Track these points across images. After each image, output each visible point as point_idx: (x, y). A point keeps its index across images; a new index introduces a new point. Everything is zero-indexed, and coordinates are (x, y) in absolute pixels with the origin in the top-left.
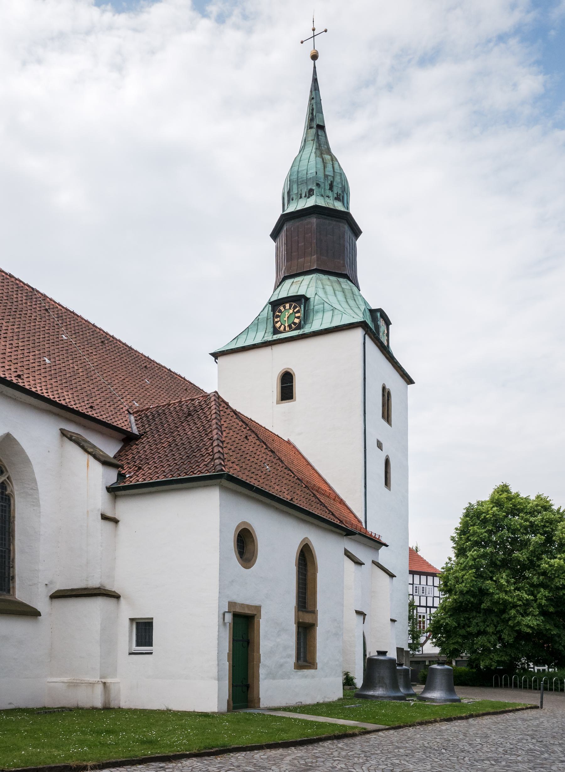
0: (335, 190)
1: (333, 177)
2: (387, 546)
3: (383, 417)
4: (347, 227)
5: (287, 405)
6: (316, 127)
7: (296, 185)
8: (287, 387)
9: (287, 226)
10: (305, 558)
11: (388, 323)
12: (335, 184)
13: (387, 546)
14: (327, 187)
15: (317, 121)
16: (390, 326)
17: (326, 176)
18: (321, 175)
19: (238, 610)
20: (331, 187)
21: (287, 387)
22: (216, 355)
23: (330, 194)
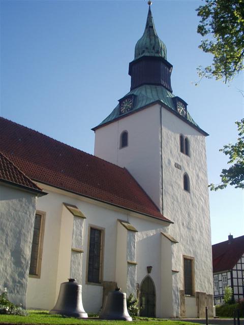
0: (156, 49)
1: (155, 44)
2: (173, 223)
3: (182, 151)
4: (162, 64)
5: (125, 149)
6: (150, 27)
7: (139, 49)
8: (124, 140)
9: (134, 68)
10: (96, 235)
11: (185, 105)
12: (156, 47)
13: (173, 223)
14: (152, 49)
15: (150, 25)
16: (187, 106)
17: (151, 44)
18: (148, 44)
19: (185, 257)
20: (154, 48)
21: (124, 140)
22: (94, 129)
23: (153, 51)
